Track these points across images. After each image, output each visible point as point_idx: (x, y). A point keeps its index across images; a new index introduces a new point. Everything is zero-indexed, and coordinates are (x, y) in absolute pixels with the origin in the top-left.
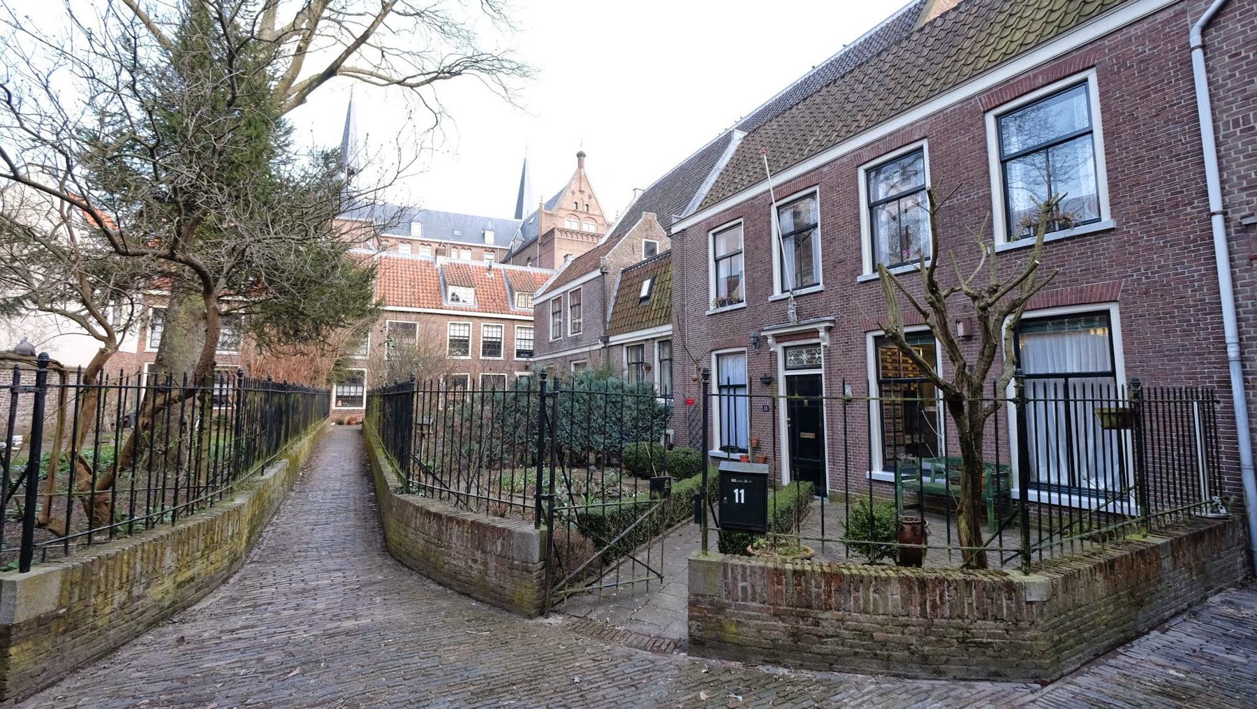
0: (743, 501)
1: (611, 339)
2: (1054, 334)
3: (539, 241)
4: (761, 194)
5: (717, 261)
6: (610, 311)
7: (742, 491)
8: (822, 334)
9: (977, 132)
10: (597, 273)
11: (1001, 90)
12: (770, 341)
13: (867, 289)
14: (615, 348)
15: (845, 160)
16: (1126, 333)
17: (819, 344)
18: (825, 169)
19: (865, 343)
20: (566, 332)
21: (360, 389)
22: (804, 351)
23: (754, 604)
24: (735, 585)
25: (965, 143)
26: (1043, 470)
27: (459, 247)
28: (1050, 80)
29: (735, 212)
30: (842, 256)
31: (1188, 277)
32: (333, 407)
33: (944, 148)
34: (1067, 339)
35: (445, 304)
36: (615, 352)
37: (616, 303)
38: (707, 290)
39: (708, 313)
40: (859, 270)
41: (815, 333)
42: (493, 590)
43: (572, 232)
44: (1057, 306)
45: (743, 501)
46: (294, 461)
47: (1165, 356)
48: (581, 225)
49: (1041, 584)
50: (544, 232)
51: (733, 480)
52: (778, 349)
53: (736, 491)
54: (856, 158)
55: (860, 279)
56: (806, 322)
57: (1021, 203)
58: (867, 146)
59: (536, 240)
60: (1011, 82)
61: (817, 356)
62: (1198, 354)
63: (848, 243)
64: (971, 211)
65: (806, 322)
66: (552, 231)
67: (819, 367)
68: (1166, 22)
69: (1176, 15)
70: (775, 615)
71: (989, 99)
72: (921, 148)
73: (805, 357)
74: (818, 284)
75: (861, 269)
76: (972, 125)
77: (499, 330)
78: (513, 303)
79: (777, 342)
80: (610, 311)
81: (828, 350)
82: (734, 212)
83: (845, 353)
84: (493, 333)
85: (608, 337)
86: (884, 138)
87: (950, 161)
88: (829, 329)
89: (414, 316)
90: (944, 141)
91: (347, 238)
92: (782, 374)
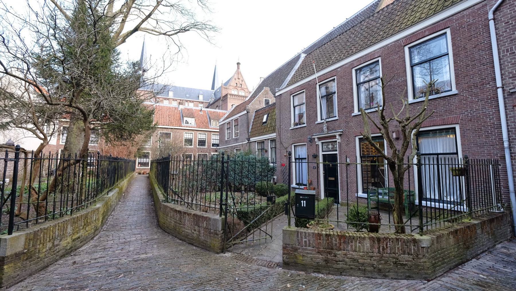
0: (305, 206)
1: (251, 139)
2: (433, 137)
3: (221, 99)
4: (312, 80)
5: (294, 107)
6: (250, 128)
7: (305, 202)
8: (337, 137)
9: (401, 54)
10: (245, 112)
11: (411, 37)
12: (316, 140)
13: (356, 118)
14: (252, 143)
15: (347, 66)
16: (462, 137)
17: (336, 141)
18: (339, 69)
19: (355, 141)
20: (232, 136)
21: (148, 160)
22: (330, 144)
23: (310, 248)
24: (302, 240)
25: (396, 59)
26: (428, 193)
27: (189, 102)
28: (431, 33)
29: (302, 87)
30: (346, 105)
31: (488, 114)
32: (137, 167)
33: (387, 61)
34: (438, 139)
35: (183, 125)
36: (252, 144)
37: (253, 125)
38: (290, 119)
39: (290, 128)
40: (353, 111)
41: (334, 137)
42: (202, 242)
43: (235, 95)
44: (434, 126)
45: (305, 206)
47: (478, 146)
48: (238, 92)
50: (223, 95)
51: (301, 197)
52: (320, 143)
53: (302, 202)
54: (351, 65)
55: (353, 114)
56: (331, 132)
57: (419, 83)
58: (356, 60)
59: (220, 99)
60: (415, 34)
61: (335, 146)
63: (348, 100)
64: (399, 87)
65: (331, 132)
66: (227, 95)
67: (336, 151)
68: (479, 9)
69: (483, 6)
71: (406, 41)
72: (378, 61)
73: (330, 146)
74: (336, 117)
75: (354, 110)
76: (399, 51)
77: (205, 135)
78: (211, 124)
79: (319, 141)
80: (250, 128)
81: (340, 144)
82: (301, 87)
83: (347, 145)
84: (202, 137)
85: (250, 138)
86: (363, 56)
87: (390, 66)
88: (340, 135)
89: (170, 130)
90: (388, 58)
92: (321, 153)
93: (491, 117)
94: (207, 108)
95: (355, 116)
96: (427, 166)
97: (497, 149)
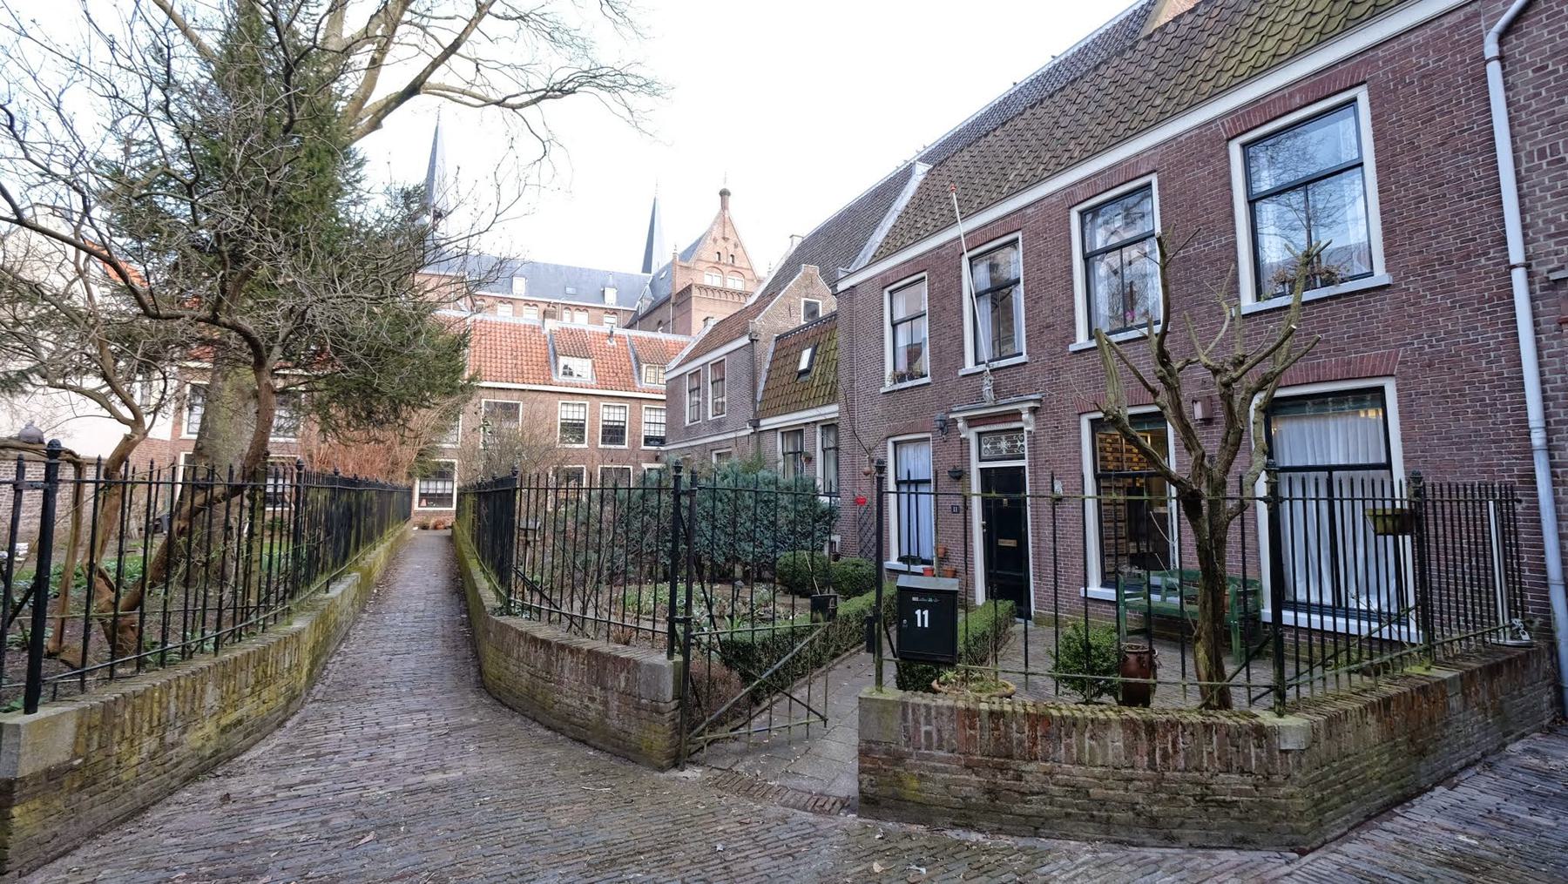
0: (926, 625)
1: (762, 423)
2: (1315, 416)
3: (672, 301)
4: (949, 242)
5: (894, 326)
6: (761, 387)
7: (926, 613)
8: (1025, 416)
9: (1218, 165)
10: (745, 340)
11: (1248, 112)
12: (960, 425)
13: (1081, 360)
14: (767, 434)
15: (1054, 199)
16: (1405, 415)
17: (1021, 429)
18: (1029, 211)
19: (1079, 428)
20: (706, 414)
21: (449, 485)
22: (1003, 437)
23: (941, 753)
24: (917, 729)
25: (1204, 178)
26: (1301, 586)
27: (573, 309)
28: (1310, 100)
29: (917, 264)
30: (1051, 320)
32: (416, 507)
33: (1177, 185)
34: (1331, 423)
35: (555, 379)
36: (767, 439)
37: (768, 378)
38: (882, 361)
39: (883, 390)
40: (1071, 337)
41: (1016, 415)
42: (615, 736)
43: (714, 290)
44: (1319, 382)
45: (926, 625)
46: (367, 575)
47: (1453, 444)
48: (724, 281)
49: (1298, 728)
50: (679, 289)
51: (914, 599)
52: (971, 435)
53: (918, 612)
54: (1068, 197)
55: (1072, 348)
56: (1006, 401)
57: (1274, 253)
58: (1081, 181)
59: (668, 299)
60: (1262, 102)
61: (1019, 444)
62: (1494, 442)
63: (1057, 303)
64: (1212, 263)
65: (1006, 401)
66: (689, 289)
67: (1022, 457)
68: (1455, 28)
69: (1467, 19)
70: (967, 767)
71: (1234, 123)
72: (1149, 185)
73: (1004, 445)
74: (1021, 354)
75: (1075, 335)
76: (1212, 156)
77: (623, 411)
78: (640, 378)
79: (970, 427)
80: (761, 387)
81: (1033, 437)
82: (915, 265)
83: (1054, 440)
84: (614, 415)
85: (758, 421)
86: (1103, 171)
87: (1185, 200)
88: (1034, 411)
89: (516, 394)
90: (1178, 175)
91: (433, 297)
92: (975, 466)
93: (1492, 354)
94: (629, 327)
95: (1080, 351)
96: (1299, 505)
97: (1510, 453)
